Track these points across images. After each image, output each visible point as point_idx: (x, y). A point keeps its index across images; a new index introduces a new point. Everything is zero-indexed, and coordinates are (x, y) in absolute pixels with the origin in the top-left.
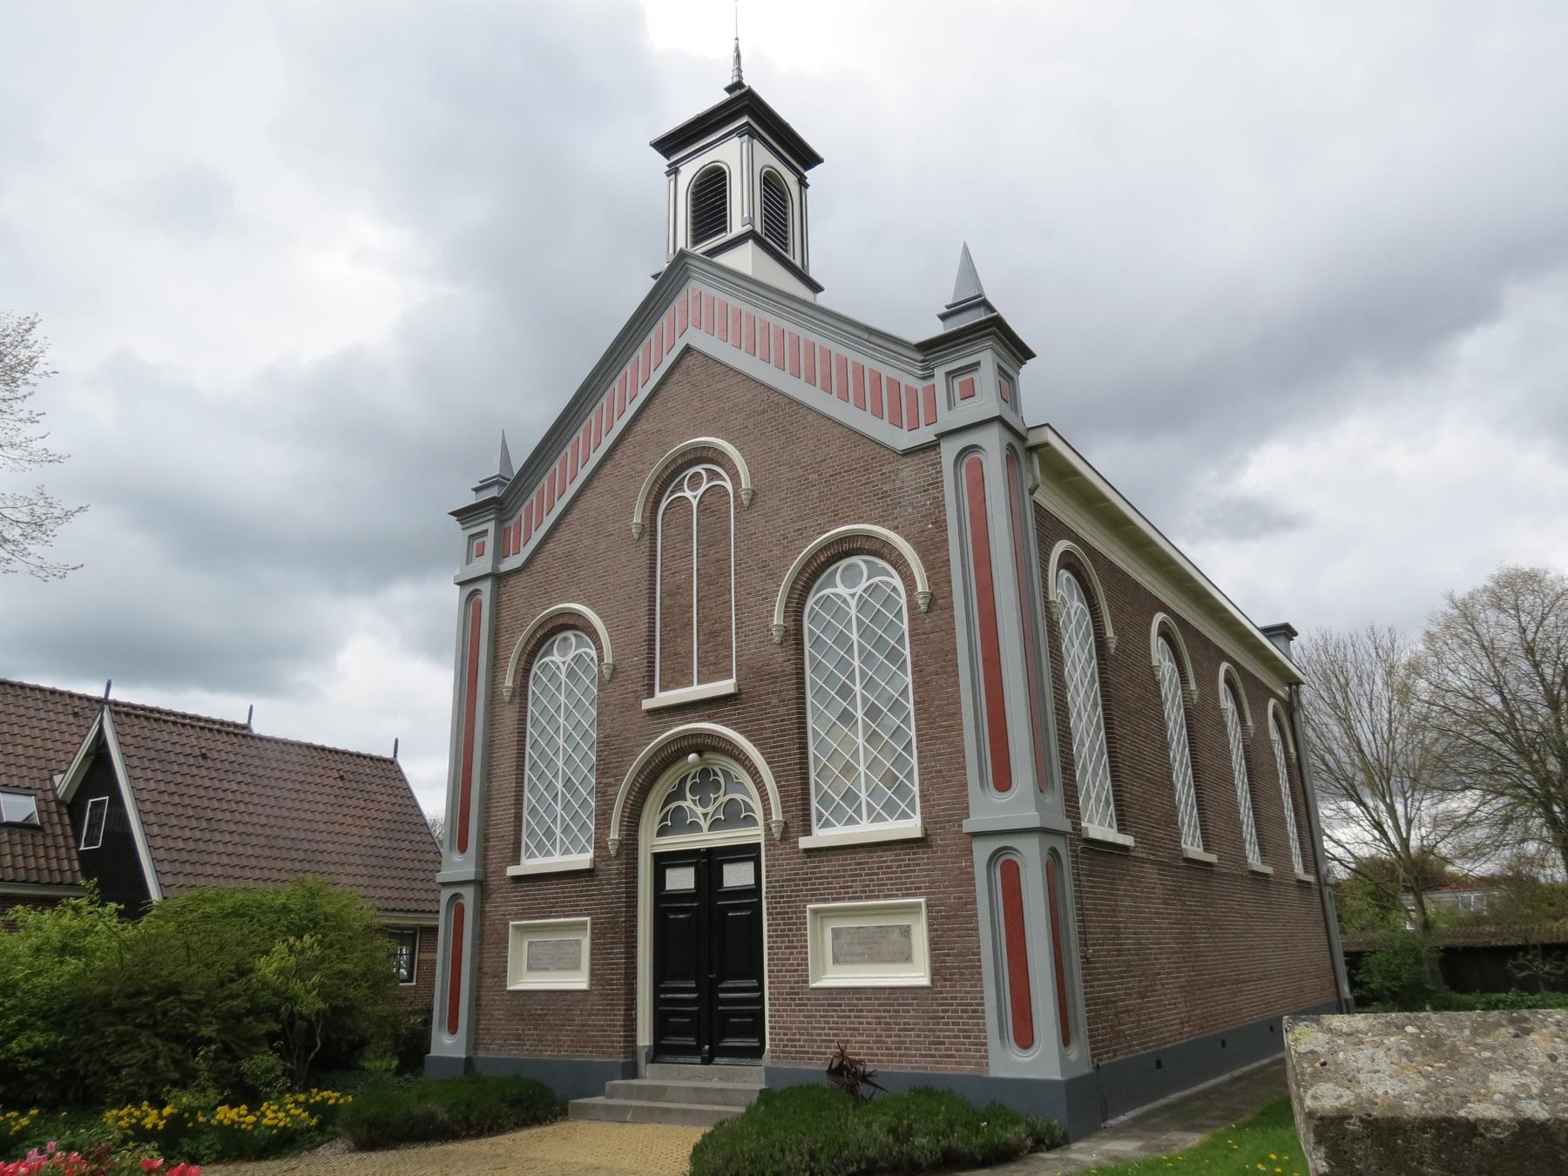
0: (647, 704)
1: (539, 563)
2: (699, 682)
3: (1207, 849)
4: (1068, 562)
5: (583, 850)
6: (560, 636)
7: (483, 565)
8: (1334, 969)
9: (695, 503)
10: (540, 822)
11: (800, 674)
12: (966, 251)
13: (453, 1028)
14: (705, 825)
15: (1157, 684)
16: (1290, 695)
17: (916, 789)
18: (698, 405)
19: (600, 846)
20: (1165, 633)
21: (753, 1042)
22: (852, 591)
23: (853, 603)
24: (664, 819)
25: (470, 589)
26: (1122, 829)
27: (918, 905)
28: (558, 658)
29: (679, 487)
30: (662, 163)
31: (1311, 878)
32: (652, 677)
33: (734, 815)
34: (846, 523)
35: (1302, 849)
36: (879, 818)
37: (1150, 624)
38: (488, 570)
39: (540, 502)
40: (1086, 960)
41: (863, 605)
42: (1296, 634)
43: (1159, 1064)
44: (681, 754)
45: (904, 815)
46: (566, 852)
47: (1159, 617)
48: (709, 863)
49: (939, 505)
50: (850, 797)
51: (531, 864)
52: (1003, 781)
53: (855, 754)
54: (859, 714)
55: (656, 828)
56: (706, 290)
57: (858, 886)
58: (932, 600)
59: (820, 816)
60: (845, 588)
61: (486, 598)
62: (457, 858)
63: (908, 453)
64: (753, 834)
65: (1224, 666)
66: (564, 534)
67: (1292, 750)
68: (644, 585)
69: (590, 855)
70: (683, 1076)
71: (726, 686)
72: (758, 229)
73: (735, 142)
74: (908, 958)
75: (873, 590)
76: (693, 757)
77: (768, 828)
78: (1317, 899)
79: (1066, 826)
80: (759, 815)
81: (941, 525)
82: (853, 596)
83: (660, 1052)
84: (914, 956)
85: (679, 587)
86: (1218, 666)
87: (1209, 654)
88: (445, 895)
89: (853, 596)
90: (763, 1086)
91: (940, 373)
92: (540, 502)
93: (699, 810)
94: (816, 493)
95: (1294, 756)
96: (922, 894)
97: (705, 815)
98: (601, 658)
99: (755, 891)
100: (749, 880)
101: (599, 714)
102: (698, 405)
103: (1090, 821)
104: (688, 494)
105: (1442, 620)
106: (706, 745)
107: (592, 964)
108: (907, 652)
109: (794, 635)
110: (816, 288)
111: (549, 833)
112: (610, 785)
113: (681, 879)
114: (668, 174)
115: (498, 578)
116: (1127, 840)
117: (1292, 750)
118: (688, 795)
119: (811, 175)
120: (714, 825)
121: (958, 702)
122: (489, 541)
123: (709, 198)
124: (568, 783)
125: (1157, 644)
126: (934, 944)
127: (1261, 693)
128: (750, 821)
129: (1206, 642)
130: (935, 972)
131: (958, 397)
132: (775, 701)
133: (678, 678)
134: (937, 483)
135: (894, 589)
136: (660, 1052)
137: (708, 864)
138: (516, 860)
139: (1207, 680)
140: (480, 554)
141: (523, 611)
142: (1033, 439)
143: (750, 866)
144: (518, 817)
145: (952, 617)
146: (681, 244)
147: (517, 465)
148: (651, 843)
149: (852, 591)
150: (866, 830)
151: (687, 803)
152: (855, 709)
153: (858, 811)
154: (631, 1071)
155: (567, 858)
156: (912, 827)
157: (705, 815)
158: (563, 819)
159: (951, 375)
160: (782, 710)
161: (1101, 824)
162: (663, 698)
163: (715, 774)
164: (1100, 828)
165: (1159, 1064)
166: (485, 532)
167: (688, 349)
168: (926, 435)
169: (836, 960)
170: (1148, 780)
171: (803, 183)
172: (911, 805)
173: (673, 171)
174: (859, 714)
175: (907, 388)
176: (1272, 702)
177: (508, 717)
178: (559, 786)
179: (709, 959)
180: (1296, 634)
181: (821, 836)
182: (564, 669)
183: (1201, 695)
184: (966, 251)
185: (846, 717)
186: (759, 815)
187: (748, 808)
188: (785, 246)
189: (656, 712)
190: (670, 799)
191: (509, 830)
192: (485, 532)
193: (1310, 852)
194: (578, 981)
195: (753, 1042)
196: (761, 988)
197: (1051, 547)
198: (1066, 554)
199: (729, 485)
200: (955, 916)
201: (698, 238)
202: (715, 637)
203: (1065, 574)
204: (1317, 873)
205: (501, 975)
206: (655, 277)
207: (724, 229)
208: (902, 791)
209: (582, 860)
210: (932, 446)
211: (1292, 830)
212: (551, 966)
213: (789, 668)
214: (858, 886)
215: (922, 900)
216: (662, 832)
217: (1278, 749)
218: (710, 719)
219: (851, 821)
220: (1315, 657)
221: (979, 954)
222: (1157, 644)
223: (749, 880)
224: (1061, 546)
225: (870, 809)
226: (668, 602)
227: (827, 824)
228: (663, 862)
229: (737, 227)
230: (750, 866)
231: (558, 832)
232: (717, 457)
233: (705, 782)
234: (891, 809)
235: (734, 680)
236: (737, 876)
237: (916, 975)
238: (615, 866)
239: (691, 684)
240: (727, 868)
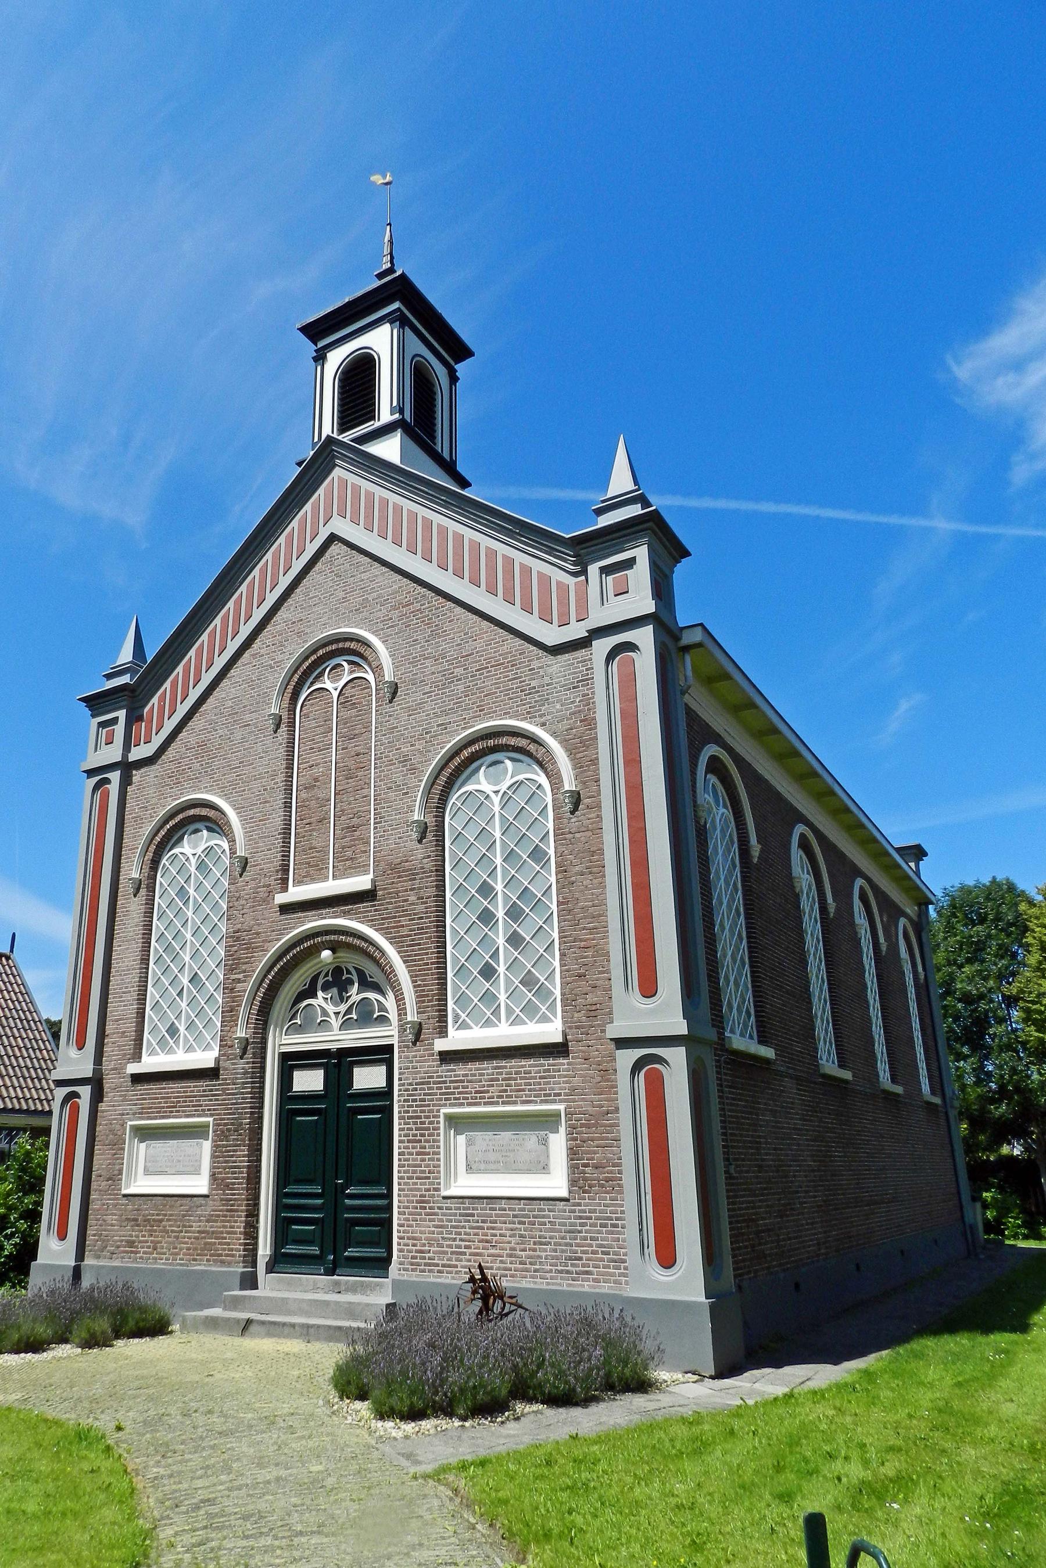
0: (281, 899)
1: (171, 752)
2: (334, 877)
3: (842, 1065)
4: (715, 766)
5: (208, 1047)
6: (192, 827)
7: (113, 753)
8: (959, 1193)
9: (335, 694)
10: (163, 1017)
11: (441, 871)
13: (62, 1236)
15: (797, 897)
16: (919, 916)
17: (558, 993)
18: (342, 594)
20: (805, 845)
21: (380, 1252)
23: (496, 799)
25: (95, 779)
26: (763, 1041)
27: (557, 1115)
28: (191, 848)
30: (309, 348)
31: (937, 1100)
32: (286, 871)
33: (366, 1016)
35: (928, 1070)
36: (516, 1021)
37: (791, 835)
38: (117, 757)
39: (161, 709)
40: (729, 1177)
41: (506, 801)
42: (926, 854)
43: (797, 1286)
44: (316, 950)
45: (545, 1019)
46: (189, 1049)
47: (800, 829)
48: (339, 1063)
49: (588, 701)
51: (151, 1062)
52: (649, 988)
53: (495, 955)
54: (500, 914)
56: (352, 479)
57: (494, 1091)
59: (457, 1017)
61: (114, 788)
62: (73, 1052)
63: (557, 650)
64: (387, 1034)
65: (859, 882)
66: (196, 722)
67: (920, 969)
68: (281, 777)
69: (215, 1053)
70: (309, 1291)
71: (361, 882)
72: (407, 416)
73: (386, 328)
74: (544, 1168)
76: (326, 954)
77: (402, 1030)
78: (943, 1122)
79: (712, 1034)
80: (393, 1015)
81: (590, 723)
82: (496, 792)
83: (278, 1262)
84: (552, 1166)
85: (316, 780)
86: (853, 882)
87: (844, 871)
88: (61, 1092)
90: (389, 1300)
91: (593, 569)
92: (161, 709)
93: (331, 1009)
94: (461, 688)
95: (922, 977)
96: (561, 1101)
97: (337, 1014)
98: (233, 851)
99: (386, 1094)
100: (382, 1083)
101: (229, 908)
102: (342, 594)
103: (732, 1031)
104: (328, 685)
106: (340, 940)
107: (213, 1167)
108: (551, 852)
109: (432, 833)
110: (464, 483)
111: (173, 1031)
112: (239, 981)
113: (309, 1081)
114: (316, 359)
116: (767, 1052)
117: (920, 969)
118: (320, 994)
119: (461, 368)
120: (346, 1025)
121: (603, 903)
122: (120, 729)
123: (358, 382)
124: (194, 979)
125: (797, 855)
126: (573, 1153)
127: (891, 910)
128: (383, 1020)
129: (842, 856)
130: (573, 1182)
131: (611, 593)
132: (412, 898)
133: (314, 872)
134: (587, 680)
136: (278, 1262)
137: (338, 1065)
138: (137, 1056)
139: (843, 894)
140: (109, 742)
141: (154, 801)
142: (688, 638)
143: (383, 1069)
144: (141, 1014)
145: (599, 816)
146: (327, 431)
147: (150, 654)
148: (281, 1041)
149: (496, 788)
150: (504, 1033)
152: (497, 908)
153: (496, 1012)
154: (250, 1281)
155: (191, 1056)
156: (551, 1031)
157: (337, 1014)
158: (188, 1016)
159: (606, 571)
160: (421, 908)
161: (742, 1035)
162: (296, 893)
163: (349, 972)
164: (743, 1041)
165: (797, 1286)
166: (115, 721)
167: (333, 538)
168: (577, 631)
169: (469, 1169)
170: (787, 992)
171: (453, 379)
172: (552, 1008)
173: (320, 357)
174: (500, 914)
175: (558, 583)
176: (902, 921)
177: (132, 908)
178: (185, 981)
180: (926, 854)
181: (457, 1039)
182: (193, 861)
183: (837, 909)
185: (487, 917)
186: (393, 1015)
187: (382, 1008)
188: (433, 438)
189: (286, 909)
190: (301, 996)
191: (131, 1027)
192: (115, 721)
193: (936, 1074)
194: (200, 1184)
195: (380, 1252)
196: (389, 1196)
197: (700, 750)
198: (713, 760)
199: (370, 677)
200: (596, 1125)
201: (344, 427)
202: (352, 829)
203: (713, 779)
204: (944, 1097)
205: (114, 1178)
206: (299, 464)
207: (373, 418)
208: (543, 993)
209: (205, 1058)
210: (583, 643)
211: (920, 1051)
212: (171, 1171)
213: (428, 864)
214: (494, 1091)
215: (561, 1107)
217: (907, 968)
218: (345, 914)
219: (488, 1023)
221: (619, 1165)
222: (797, 855)
223: (382, 1083)
224: (712, 750)
225: (509, 1011)
226: (304, 795)
227: (464, 1026)
228: (291, 1062)
229: (385, 415)
230: (383, 1069)
231: (182, 1029)
234: (530, 1010)
235: (371, 876)
236: (367, 1078)
237: (555, 1183)
238: (241, 1065)
239: (326, 878)
240: (357, 1071)
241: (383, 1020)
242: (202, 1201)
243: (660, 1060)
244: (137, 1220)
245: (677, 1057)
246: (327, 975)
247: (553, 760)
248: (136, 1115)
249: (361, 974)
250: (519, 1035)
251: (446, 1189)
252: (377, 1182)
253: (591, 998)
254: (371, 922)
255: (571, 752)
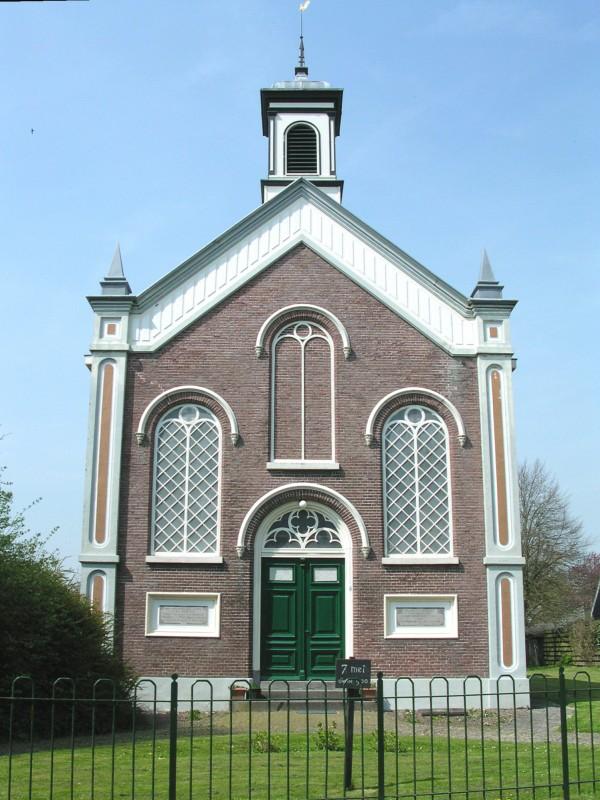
2: (305, 458)
9: (303, 345)
12: (486, 258)
14: (303, 544)
19: (227, 549)
22: (415, 424)
24: (271, 537)
27: (453, 598)
29: (290, 330)
34: (186, 384)
41: (422, 436)
48: (304, 567)
50: (410, 538)
52: (504, 541)
55: (265, 543)
58: (468, 444)
60: (186, 423)
75: (203, 426)
82: (189, 425)
89: (189, 425)
98: (227, 430)
105: (540, 498)
113: (284, 575)
115: (133, 357)
132: (365, 478)
135: (215, 428)
148: (261, 551)
150: (419, 557)
151: (290, 529)
153: (415, 546)
156: (449, 558)
179: (293, 628)
184: (486, 258)
190: (275, 525)
199: (330, 340)
215: (456, 596)
216: (269, 545)
218: (318, 482)
220: (24, 529)
232: (325, 323)
233: (303, 521)
236: (324, 576)
239: (300, 457)
241: (337, 545)
242: (215, 641)
243: (511, 575)
244: (159, 651)
245: (519, 574)
246: (295, 514)
247: (218, 405)
248: (152, 588)
249: (320, 516)
250: (427, 559)
251: (388, 635)
252: (333, 632)
253: (472, 543)
254: (333, 487)
255: (463, 415)
